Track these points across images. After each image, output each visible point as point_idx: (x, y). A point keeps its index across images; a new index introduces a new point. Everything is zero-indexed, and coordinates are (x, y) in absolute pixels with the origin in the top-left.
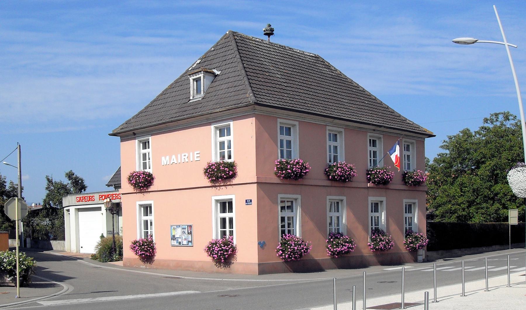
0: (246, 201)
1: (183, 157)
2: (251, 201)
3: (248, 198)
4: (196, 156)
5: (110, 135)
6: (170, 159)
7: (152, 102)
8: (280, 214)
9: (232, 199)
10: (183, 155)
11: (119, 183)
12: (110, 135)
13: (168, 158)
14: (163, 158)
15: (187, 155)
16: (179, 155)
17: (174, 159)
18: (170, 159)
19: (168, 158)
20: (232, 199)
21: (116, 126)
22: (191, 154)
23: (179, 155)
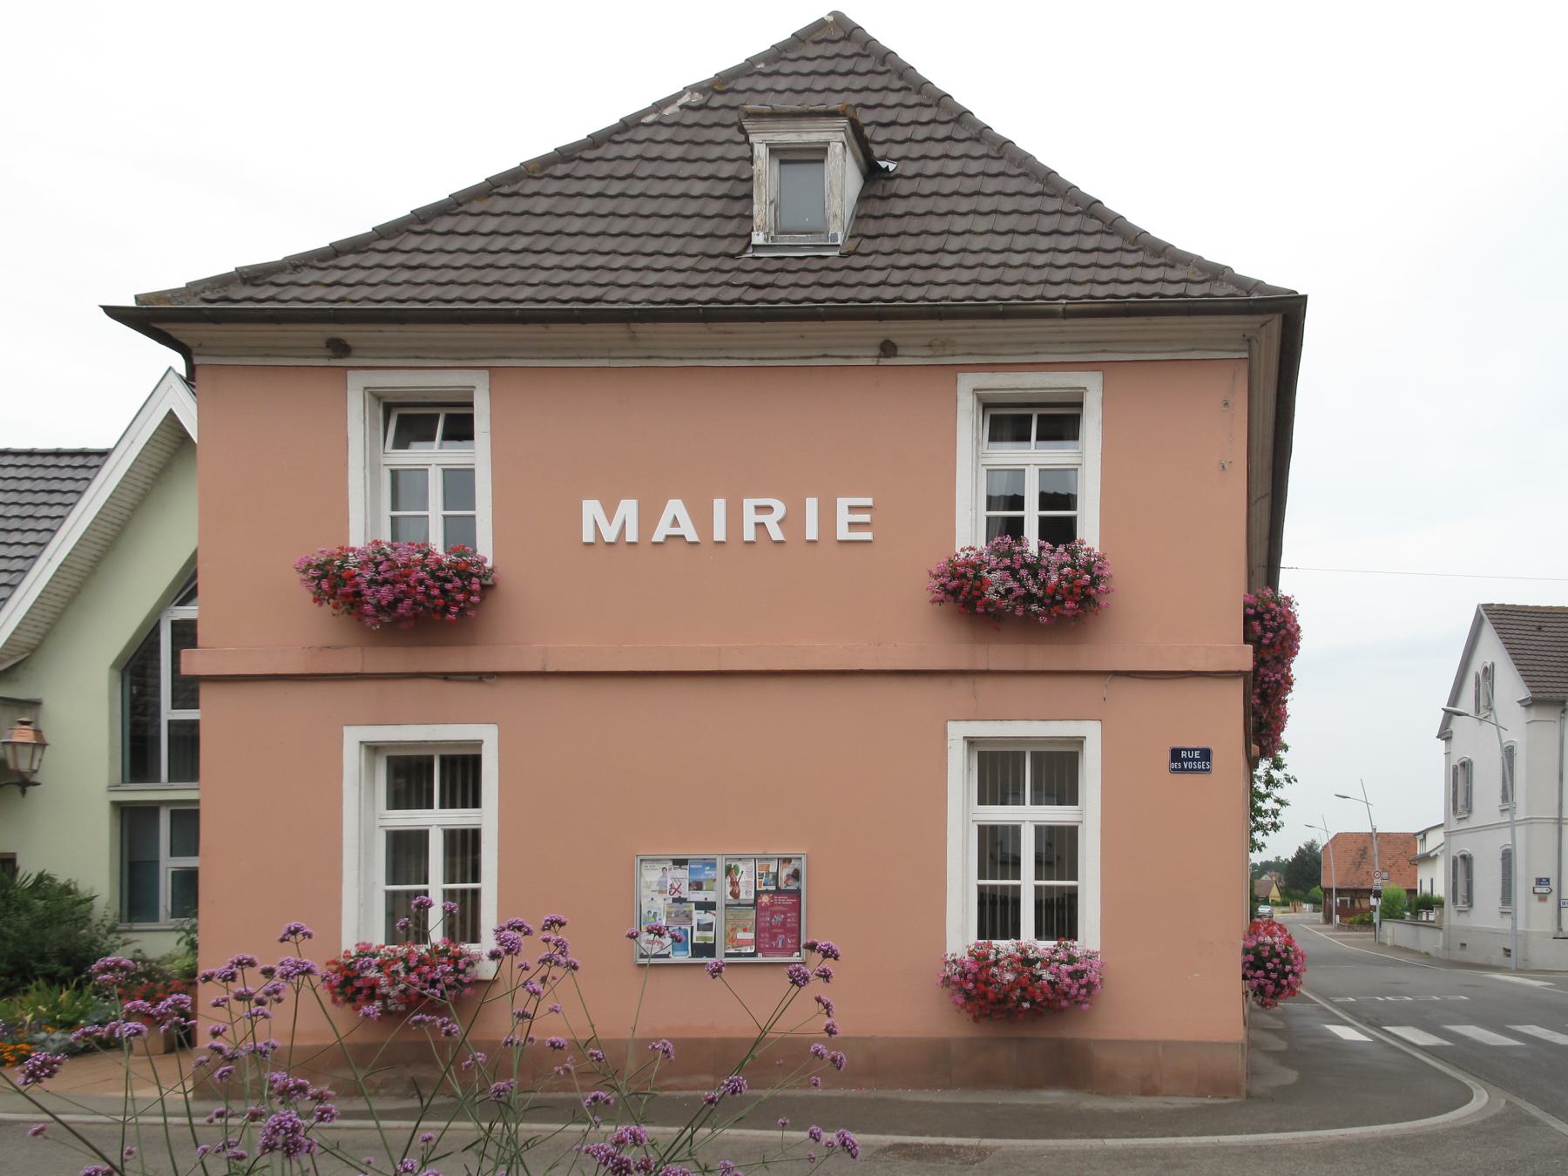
0: (1176, 754)
1: (750, 518)
2: (1206, 754)
3: (1190, 740)
4: (843, 517)
5: (114, 312)
6: (648, 518)
7: (383, 232)
8: (486, 818)
9: (478, 744)
10: (749, 505)
11: (459, 837)
12: (114, 312)
13: (628, 509)
14: (591, 509)
15: (780, 509)
16: (719, 506)
17: (676, 517)
18: (648, 518)
19: (628, 509)
20: (478, 744)
21: (173, 270)
22: (812, 505)
23: (719, 506)
